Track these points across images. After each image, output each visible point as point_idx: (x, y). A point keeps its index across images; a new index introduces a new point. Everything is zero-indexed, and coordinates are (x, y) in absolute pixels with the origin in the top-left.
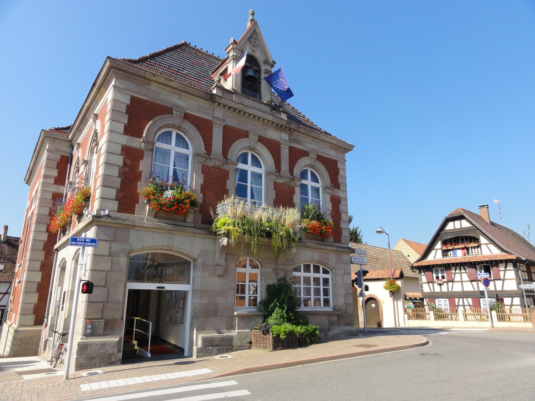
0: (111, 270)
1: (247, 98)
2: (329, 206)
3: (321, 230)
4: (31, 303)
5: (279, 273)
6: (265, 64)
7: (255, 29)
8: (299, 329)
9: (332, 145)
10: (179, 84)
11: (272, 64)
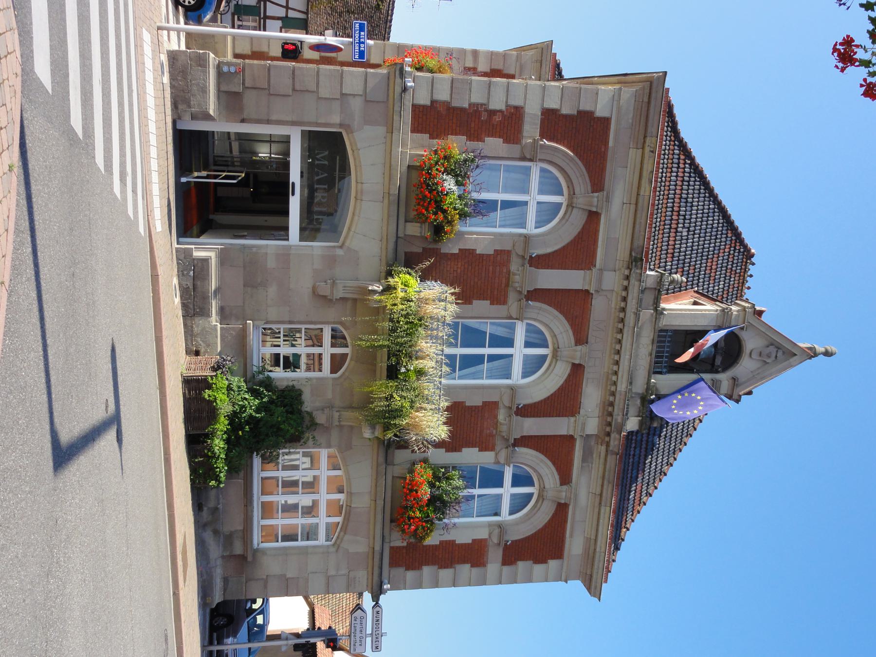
0: (320, 98)
1: (653, 340)
2: (463, 538)
3: (411, 508)
4: (269, 47)
5: (323, 413)
6: (731, 381)
7: (796, 355)
8: (218, 444)
9: (593, 542)
10: (647, 198)
11: (735, 397)
